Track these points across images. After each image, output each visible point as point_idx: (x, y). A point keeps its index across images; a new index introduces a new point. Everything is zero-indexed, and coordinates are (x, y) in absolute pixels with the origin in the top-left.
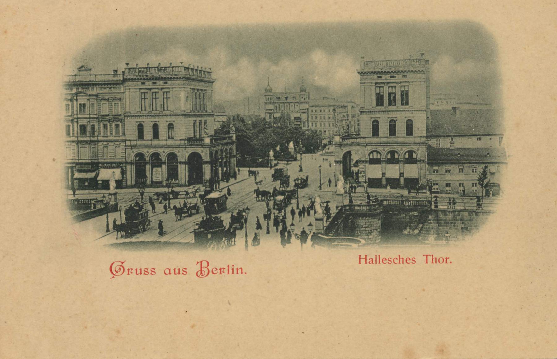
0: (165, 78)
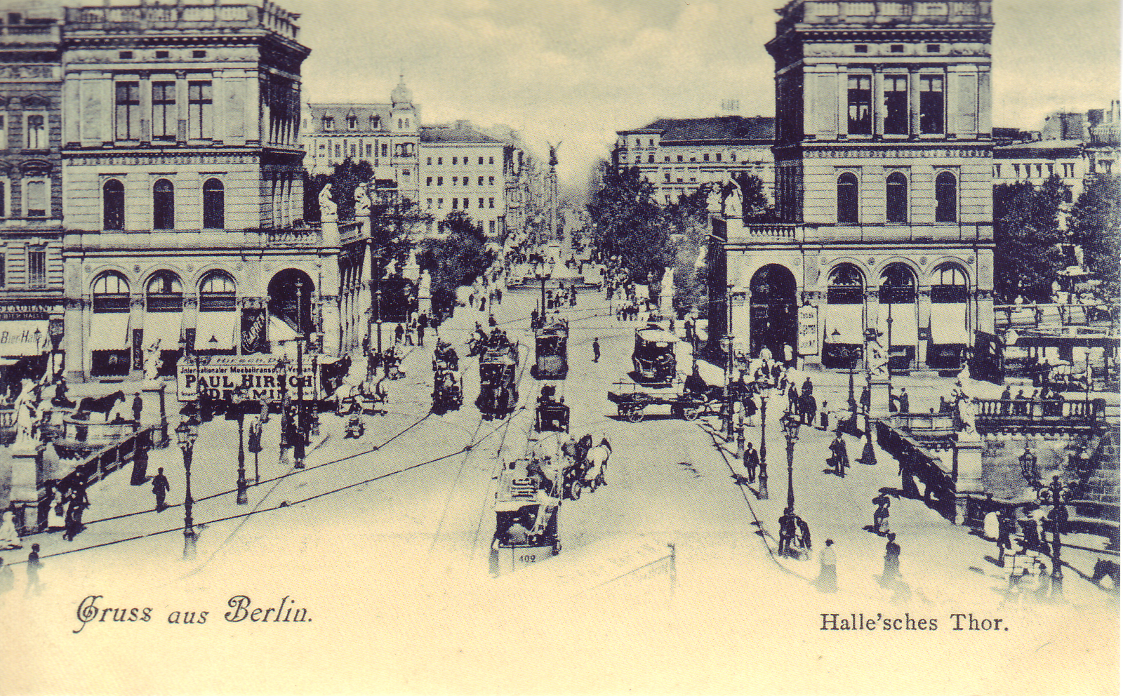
0: (161, 41)
